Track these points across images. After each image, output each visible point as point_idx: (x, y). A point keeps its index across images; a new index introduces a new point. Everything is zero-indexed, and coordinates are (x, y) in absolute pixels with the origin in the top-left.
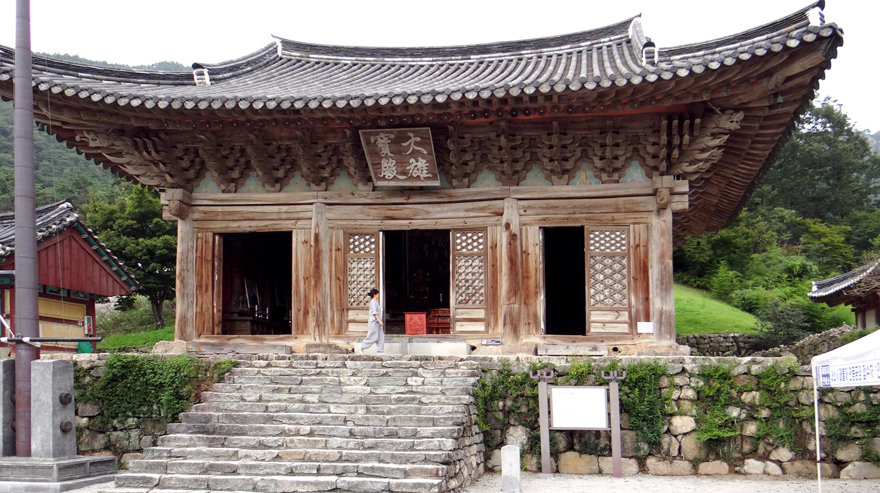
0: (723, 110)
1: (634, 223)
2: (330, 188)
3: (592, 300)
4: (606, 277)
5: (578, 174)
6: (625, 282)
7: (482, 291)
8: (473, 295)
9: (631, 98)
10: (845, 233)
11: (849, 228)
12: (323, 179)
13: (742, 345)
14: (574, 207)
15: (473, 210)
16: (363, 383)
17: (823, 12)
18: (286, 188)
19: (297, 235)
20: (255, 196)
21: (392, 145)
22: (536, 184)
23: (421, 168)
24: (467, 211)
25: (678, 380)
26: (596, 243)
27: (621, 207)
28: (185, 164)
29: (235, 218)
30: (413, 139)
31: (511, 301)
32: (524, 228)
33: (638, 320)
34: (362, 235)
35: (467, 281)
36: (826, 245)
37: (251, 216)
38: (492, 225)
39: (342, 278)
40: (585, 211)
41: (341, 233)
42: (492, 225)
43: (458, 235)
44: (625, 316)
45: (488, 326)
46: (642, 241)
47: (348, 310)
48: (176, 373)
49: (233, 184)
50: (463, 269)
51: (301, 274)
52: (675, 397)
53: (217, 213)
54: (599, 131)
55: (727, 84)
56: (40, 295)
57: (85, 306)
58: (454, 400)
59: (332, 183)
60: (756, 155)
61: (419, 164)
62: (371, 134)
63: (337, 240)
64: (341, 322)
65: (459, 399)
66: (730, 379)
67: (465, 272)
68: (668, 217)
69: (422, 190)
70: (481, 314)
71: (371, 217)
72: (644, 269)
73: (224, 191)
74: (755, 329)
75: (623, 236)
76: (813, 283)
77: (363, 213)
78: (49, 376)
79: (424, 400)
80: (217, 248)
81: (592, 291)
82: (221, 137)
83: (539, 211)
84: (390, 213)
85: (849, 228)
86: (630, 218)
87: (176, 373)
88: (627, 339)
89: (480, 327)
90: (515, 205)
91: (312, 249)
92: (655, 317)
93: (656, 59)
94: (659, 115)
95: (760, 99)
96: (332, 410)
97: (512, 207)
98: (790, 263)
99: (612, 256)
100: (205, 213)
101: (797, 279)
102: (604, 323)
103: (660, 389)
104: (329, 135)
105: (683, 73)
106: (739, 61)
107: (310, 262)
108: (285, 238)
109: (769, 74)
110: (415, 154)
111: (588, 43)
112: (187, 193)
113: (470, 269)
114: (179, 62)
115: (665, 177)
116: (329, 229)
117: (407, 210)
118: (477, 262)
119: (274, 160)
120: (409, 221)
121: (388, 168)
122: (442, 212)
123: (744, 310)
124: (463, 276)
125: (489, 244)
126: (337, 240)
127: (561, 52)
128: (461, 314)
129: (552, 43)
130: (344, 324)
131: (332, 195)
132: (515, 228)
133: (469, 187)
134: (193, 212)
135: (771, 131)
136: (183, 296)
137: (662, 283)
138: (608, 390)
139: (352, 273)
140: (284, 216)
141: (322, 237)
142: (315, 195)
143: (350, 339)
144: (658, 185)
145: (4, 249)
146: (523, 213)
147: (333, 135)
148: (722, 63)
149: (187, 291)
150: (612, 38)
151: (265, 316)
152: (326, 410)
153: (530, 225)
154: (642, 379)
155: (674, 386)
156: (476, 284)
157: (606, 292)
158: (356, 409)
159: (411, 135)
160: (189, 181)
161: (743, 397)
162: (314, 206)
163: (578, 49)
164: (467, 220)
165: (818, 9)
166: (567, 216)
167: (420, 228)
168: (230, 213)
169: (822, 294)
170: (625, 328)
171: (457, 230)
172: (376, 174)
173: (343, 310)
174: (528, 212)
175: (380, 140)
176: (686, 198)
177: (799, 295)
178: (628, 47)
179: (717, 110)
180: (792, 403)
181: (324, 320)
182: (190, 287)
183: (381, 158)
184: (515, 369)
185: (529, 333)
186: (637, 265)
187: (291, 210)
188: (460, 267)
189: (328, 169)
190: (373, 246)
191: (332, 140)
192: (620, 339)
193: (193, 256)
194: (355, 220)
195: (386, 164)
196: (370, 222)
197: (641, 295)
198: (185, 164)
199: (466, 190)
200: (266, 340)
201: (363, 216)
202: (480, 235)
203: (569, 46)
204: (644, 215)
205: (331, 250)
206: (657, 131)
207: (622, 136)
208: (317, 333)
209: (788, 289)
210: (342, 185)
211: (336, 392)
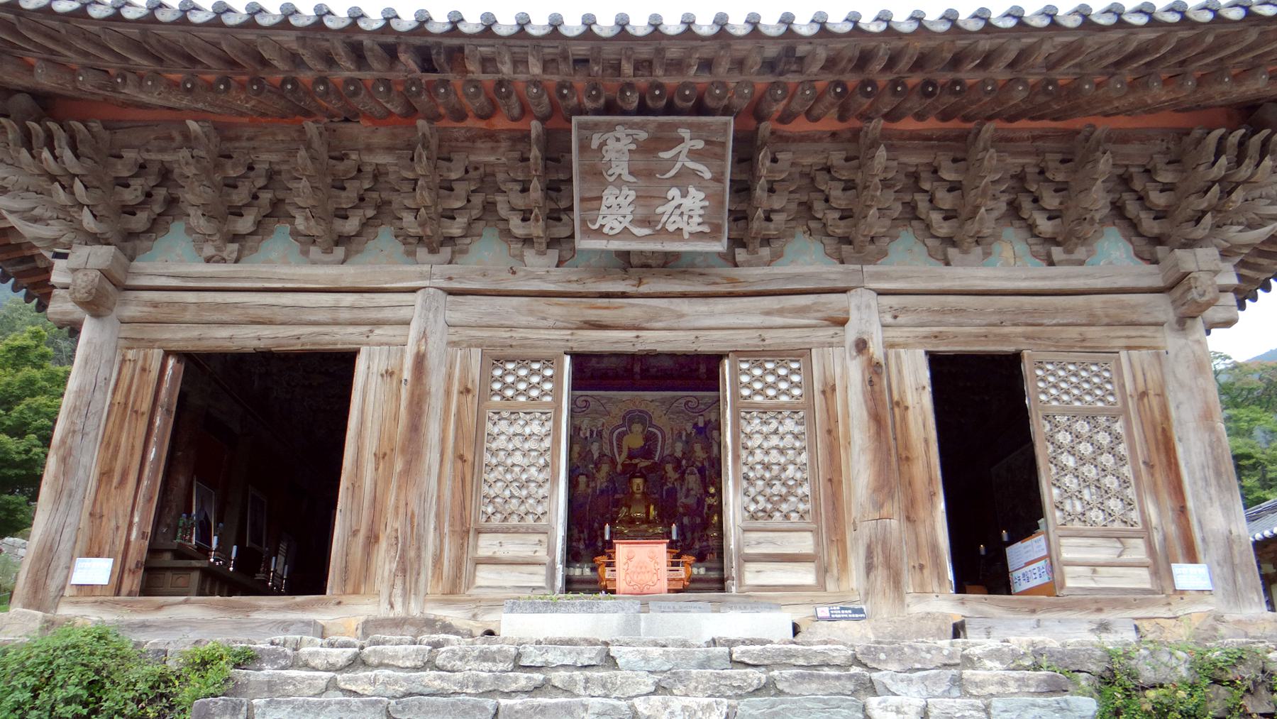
1: (1129, 348)
2: (458, 258)
5: (996, 247)
6: (1127, 471)
7: (806, 489)
8: (784, 499)
9: (1179, 70)
12: (450, 240)
14: (1000, 312)
15: (781, 312)
18: (358, 258)
20: (284, 271)
21: (636, 156)
22: (908, 262)
23: (688, 211)
24: (768, 313)
26: (1049, 391)
27: (1099, 312)
28: (131, 196)
29: (225, 317)
30: (684, 148)
31: (884, 512)
32: (892, 352)
33: (1170, 559)
34: (522, 361)
37: (265, 313)
38: (822, 345)
39: (469, 456)
40: (1023, 319)
41: (476, 354)
42: (822, 345)
43: (744, 366)
44: (1137, 550)
45: (823, 572)
46: (1150, 384)
48: (35, 692)
49: (235, 246)
50: (758, 440)
51: (370, 446)
53: (184, 306)
59: (464, 252)
61: (687, 203)
62: (595, 127)
63: (465, 370)
64: (458, 564)
67: (759, 451)
69: (668, 264)
71: (550, 323)
72: (1165, 445)
73: (208, 260)
77: (531, 312)
82: (230, 139)
83: (925, 317)
84: (593, 315)
86: (1117, 337)
87: (35, 692)
88: (1153, 603)
89: (804, 575)
90: (874, 304)
91: (405, 393)
92: (1212, 553)
97: (868, 306)
99: (1091, 417)
102: (1094, 566)
104: (479, 144)
107: (396, 418)
108: (339, 366)
110: (684, 179)
112: (123, 259)
113: (775, 441)
116: (442, 353)
117: (632, 310)
118: (789, 425)
119: (343, 194)
120: (634, 333)
121: (614, 210)
122: (712, 314)
124: (759, 455)
125: (817, 386)
126: (465, 370)
131: (466, 272)
132: (876, 350)
134: (125, 303)
136: (58, 495)
139: (494, 446)
140: (345, 315)
141: (433, 361)
142: (429, 271)
146: (888, 319)
147: (489, 145)
151: (226, 564)
153: (905, 346)
159: (685, 133)
160: (130, 235)
162: (418, 297)
164: (767, 334)
166: (983, 330)
167: (661, 348)
168: (218, 307)
170: (1141, 579)
171: (741, 354)
172: (583, 222)
173: (466, 531)
174: (901, 320)
175: (611, 144)
181: (419, 556)
182: (81, 473)
183: (605, 184)
185: (922, 591)
186: (1150, 435)
187: (364, 303)
188: (749, 436)
189: (461, 220)
191: (484, 156)
192: (1139, 604)
193: (104, 400)
194: (511, 328)
196: (544, 334)
197: (1168, 503)
198: (131, 196)
199: (766, 270)
200: (257, 608)
201: (531, 320)
204: (1149, 331)
205: (448, 393)
208: (398, 590)
210: (486, 257)
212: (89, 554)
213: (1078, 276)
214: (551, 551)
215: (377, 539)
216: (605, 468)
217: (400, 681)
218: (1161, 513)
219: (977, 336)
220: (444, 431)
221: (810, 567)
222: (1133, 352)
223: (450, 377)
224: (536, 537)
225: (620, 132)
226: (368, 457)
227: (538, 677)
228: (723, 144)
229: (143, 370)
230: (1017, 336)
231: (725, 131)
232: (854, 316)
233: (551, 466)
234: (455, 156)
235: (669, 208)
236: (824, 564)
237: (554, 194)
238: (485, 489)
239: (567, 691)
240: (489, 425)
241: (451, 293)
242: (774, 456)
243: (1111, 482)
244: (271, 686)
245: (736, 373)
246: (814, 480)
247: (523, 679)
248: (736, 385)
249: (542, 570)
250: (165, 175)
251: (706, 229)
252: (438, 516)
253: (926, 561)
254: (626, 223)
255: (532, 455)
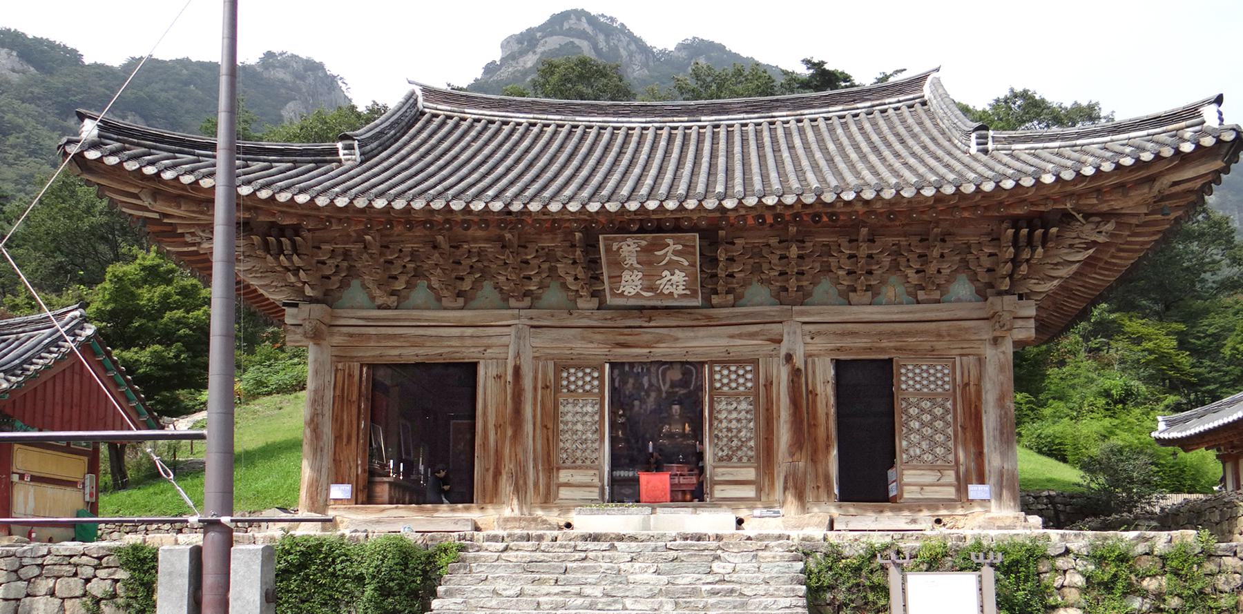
0: (1087, 216)
3: (904, 456)
4: (923, 424)
6: (950, 431)
7: (752, 443)
8: (739, 448)
10: (1176, 333)
11: (1182, 327)
13: (1061, 507)
15: (740, 336)
16: (653, 570)
17: (1221, 109)
19: (486, 367)
23: (675, 283)
24: (732, 337)
25: (1060, 563)
26: (912, 380)
30: (672, 247)
31: (795, 458)
33: (968, 481)
34: (579, 368)
35: (729, 430)
36: (1151, 352)
38: (765, 356)
39: (550, 425)
41: (551, 365)
43: (717, 369)
44: (950, 476)
45: (759, 490)
47: (558, 469)
52: (1057, 584)
54: (919, 238)
55: (1098, 191)
56: (702, 500)
57: (86, 459)
58: (787, 591)
60: (1115, 264)
61: (675, 278)
62: (614, 240)
63: (545, 374)
64: (548, 487)
65: (793, 590)
66: (1127, 561)
67: (729, 417)
68: (1008, 348)
70: (750, 474)
74: (1079, 485)
75: (946, 371)
76: (1160, 418)
77: (583, 339)
78: (257, 567)
79: (747, 591)
80: (364, 383)
81: (904, 443)
84: (621, 339)
85: (1182, 327)
89: (750, 492)
90: (799, 331)
91: (509, 391)
92: (992, 479)
93: (990, 146)
94: (1002, 219)
95: (1137, 205)
96: (628, 606)
98: (1108, 384)
99: (932, 398)
100: (351, 335)
101: (1120, 406)
102: (922, 486)
103: (1038, 574)
104: (544, 236)
105: (1048, 179)
106: (1119, 167)
107: (505, 404)
108: (472, 368)
109: (1151, 179)
110: (671, 266)
111: (868, 104)
113: (734, 415)
114: (21, 30)
115: (1006, 298)
117: (647, 335)
118: (744, 406)
122: (695, 338)
123: (1040, 452)
124: (724, 424)
125: (762, 381)
126: (545, 374)
127: (829, 115)
128: (723, 473)
129: (816, 103)
130: (553, 488)
132: (799, 361)
133: (733, 306)
135: (1141, 239)
137: (1002, 433)
138: (980, 576)
143: (565, 509)
144: (999, 308)
145: (8, 381)
146: (809, 340)
148: (1098, 169)
149: (321, 444)
150: (901, 98)
152: (620, 607)
153: (818, 356)
154: (1016, 562)
155: (1057, 571)
156: (743, 434)
157: (924, 445)
158: (661, 603)
159: (668, 241)
161: (1145, 583)
163: (854, 112)
165: (1214, 107)
169: (1175, 434)
170: (950, 493)
171: (712, 363)
172: (611, 289)
175: (625, 248)
176: (1032, 323)
177: (1124, 430)
178: (926, 111)
179: (1079, 217)
180: (1208, 590)
183: (624, 269)
184: (846, 552)
188: (719, 412)
190: (596, 383)
191: (547, 243)
195: (628, 277)
197: (972, 450)
199: (731, 310)
202: (749, 368)
203: (840, 108)
205: (535, 388)
206: (996, 239)
207: (950, 244)
209: (1107, 422)
211: (620, 583)
212: (337, 483)
213: (932, 311)
214: (601, 480)
215: (501, 473)
216: (653, 395)
217: (528, 556)
218: (966, 456)
219: (865, 349)
220: (534, 411)
221: (753, 487)
222: (964, 358)
223: (535, 378)
224: (592, 472)
225: (629, 241)
226: (491, 426)
227: (583, 555)
228: (694, 247)
229: (350, 375)
230: (891, 348)
231: (695, 241)
232: (786, 338)
233: (600, 431)
234: (529, 245)
235: (664, 281)
236: (763, 485)
237: (593, 265)
238: (561, 444)
239: (595, 560)
240: (561, 408)
241: (532, 327)
242: (734, 425)
243: (939, 438)
244: (476, 559)
245: (712, 373)
246: (757, 436)
247: (577, 555)
248: (712, 380)
249: (597, 490)
250: (346, 254)
251: (688, 292)
252: (535, 459)
253: (821, 484)
254: (638, 289)
255: (586, 421)
